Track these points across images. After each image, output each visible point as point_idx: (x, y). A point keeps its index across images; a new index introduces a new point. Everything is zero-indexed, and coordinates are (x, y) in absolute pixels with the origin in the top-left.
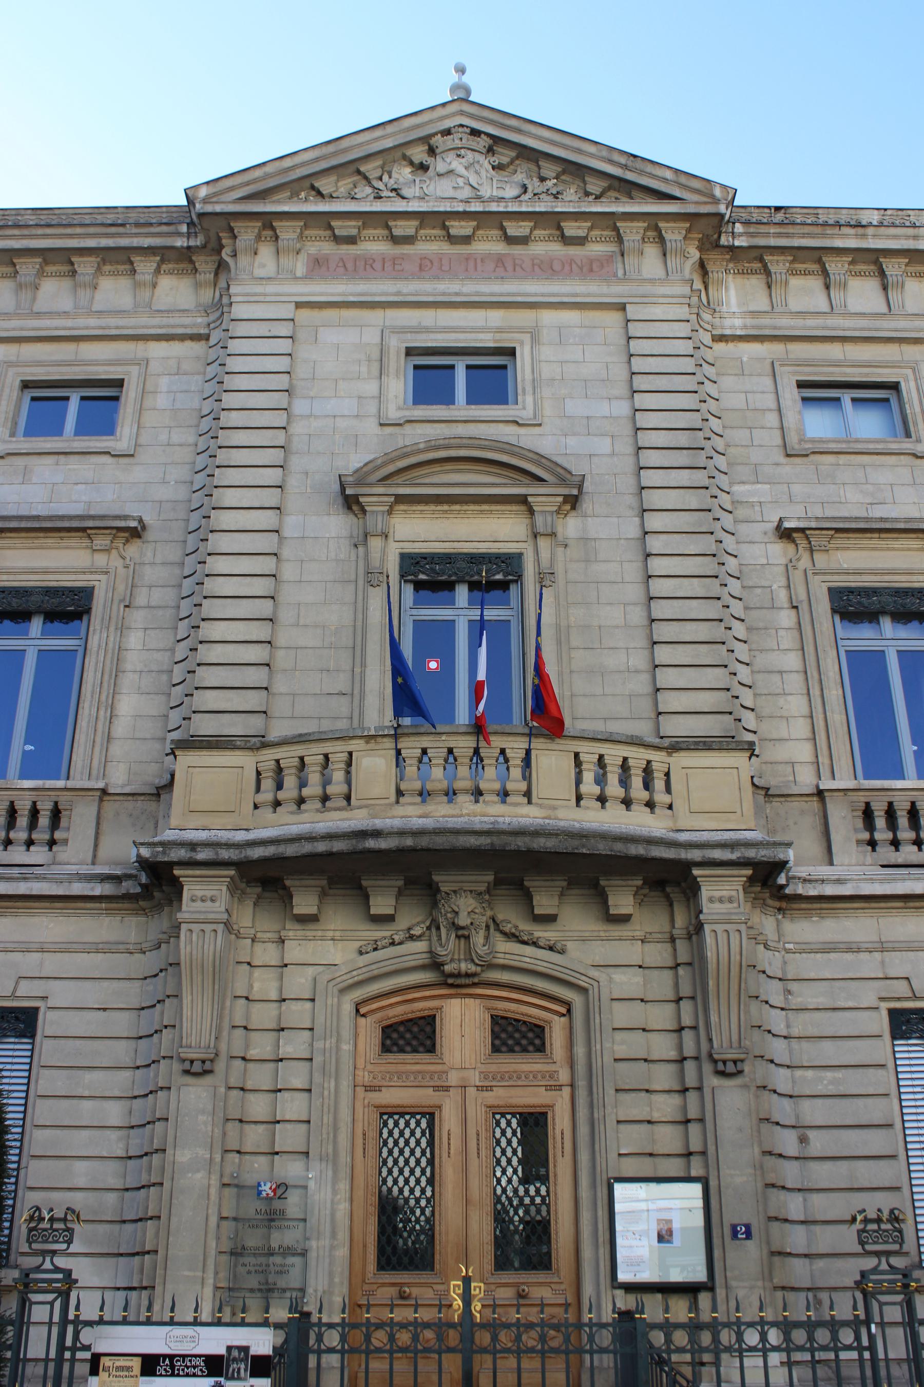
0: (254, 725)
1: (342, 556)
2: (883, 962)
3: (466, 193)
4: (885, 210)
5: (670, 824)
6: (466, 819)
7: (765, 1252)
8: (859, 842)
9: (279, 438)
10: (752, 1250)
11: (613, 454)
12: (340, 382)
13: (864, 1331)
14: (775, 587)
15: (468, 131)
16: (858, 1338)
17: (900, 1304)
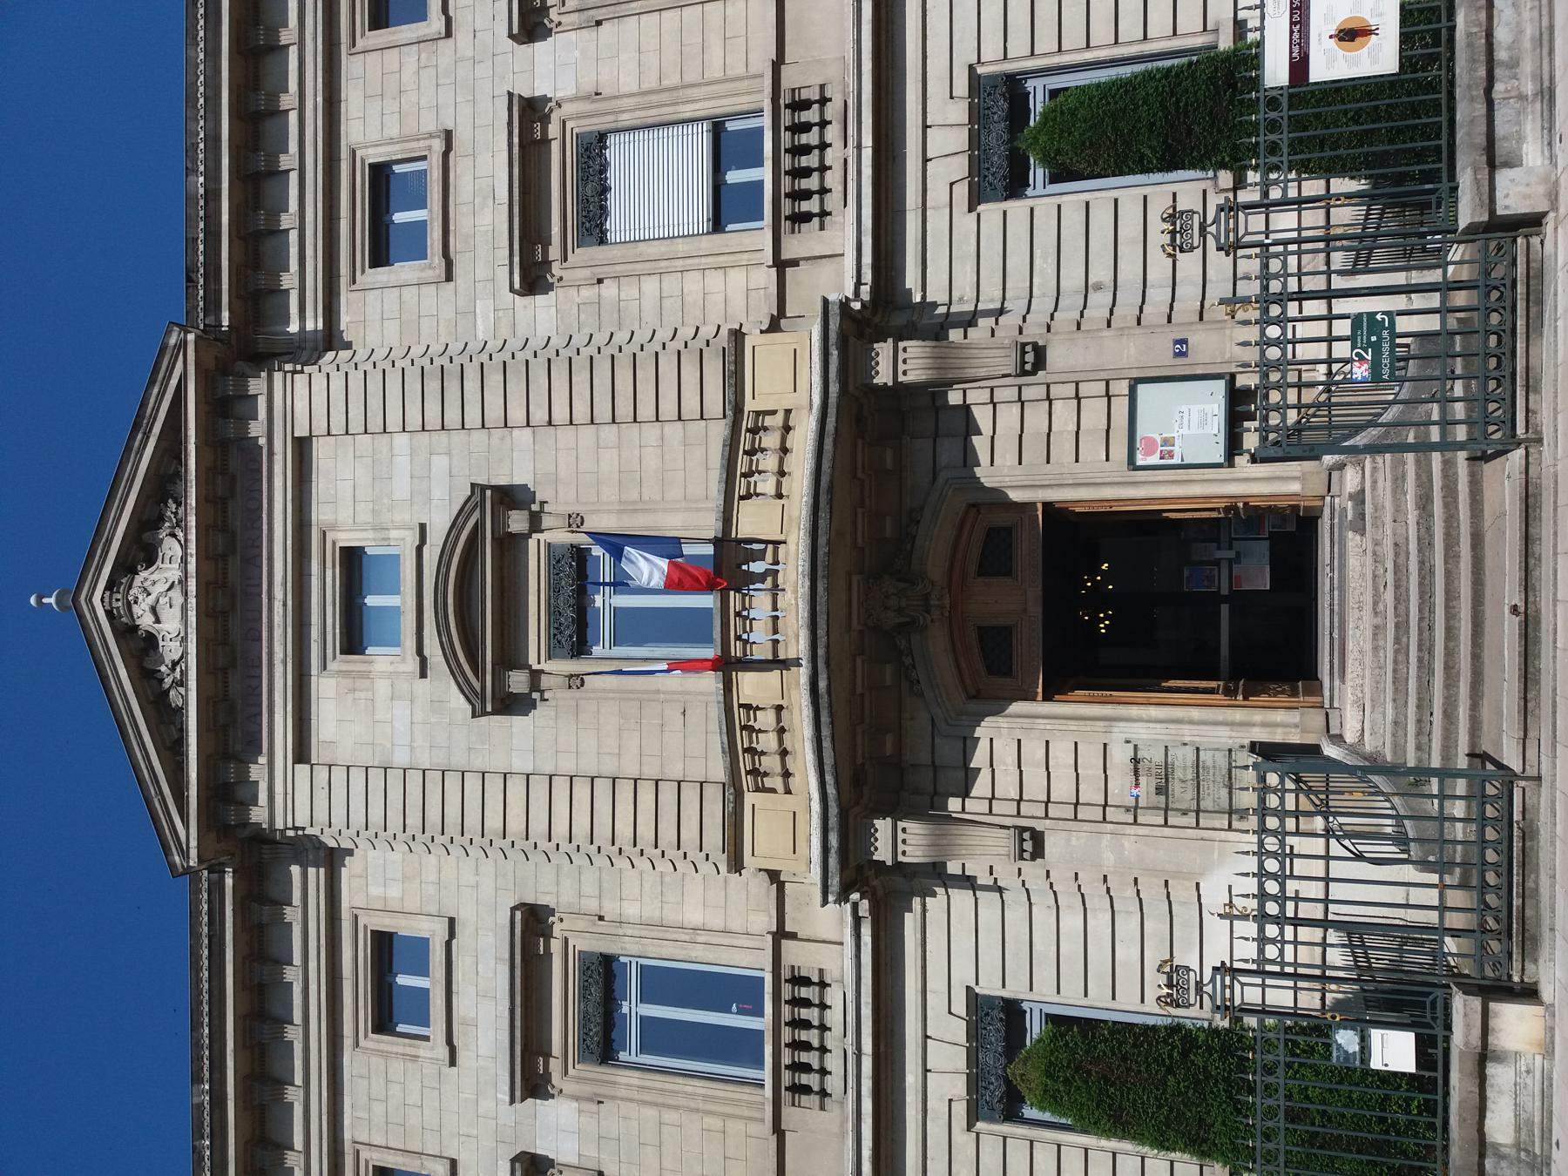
0: (714, 796)
1: (553, 714)
3: (176, 595)
5: (805, 411)
6: (800, 602)
7: (1199, 326)
8: (822, 228)
9: (434, 779)
10: (1197, 338)
11: (449, 454)
12: (377, 717)
13: (1272, 249)
16: (1276, 255)
17: (1247, 215)
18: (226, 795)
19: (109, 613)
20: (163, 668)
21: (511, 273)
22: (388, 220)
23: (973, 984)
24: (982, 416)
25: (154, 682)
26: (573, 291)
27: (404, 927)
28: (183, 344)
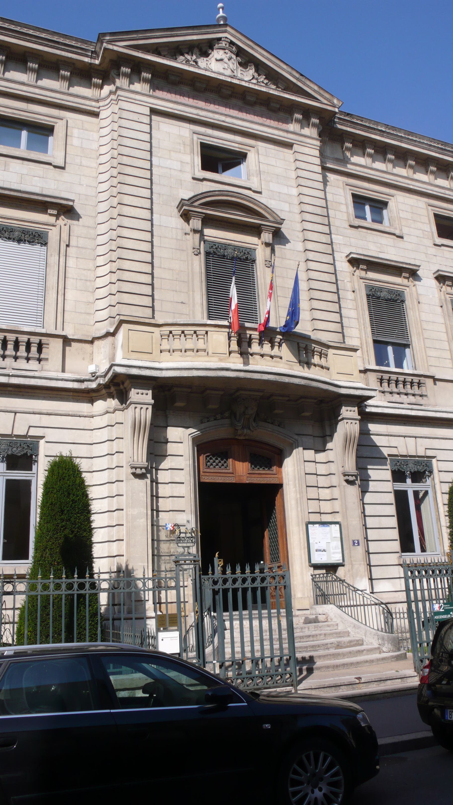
2: (388, 440)
3: (228, 72)
4: (388, 125)
14: (346, 281)
15: (229, 41)
18: (137, 68)
19: (219, 39)
20: (194, 57)
21: (357, 254)
22: (369, 206)
23: (47, 439)
24: (321, 457)
25: (187, 51)
26: (349, 279)
27: (55, 142)
28: (334, 106)
